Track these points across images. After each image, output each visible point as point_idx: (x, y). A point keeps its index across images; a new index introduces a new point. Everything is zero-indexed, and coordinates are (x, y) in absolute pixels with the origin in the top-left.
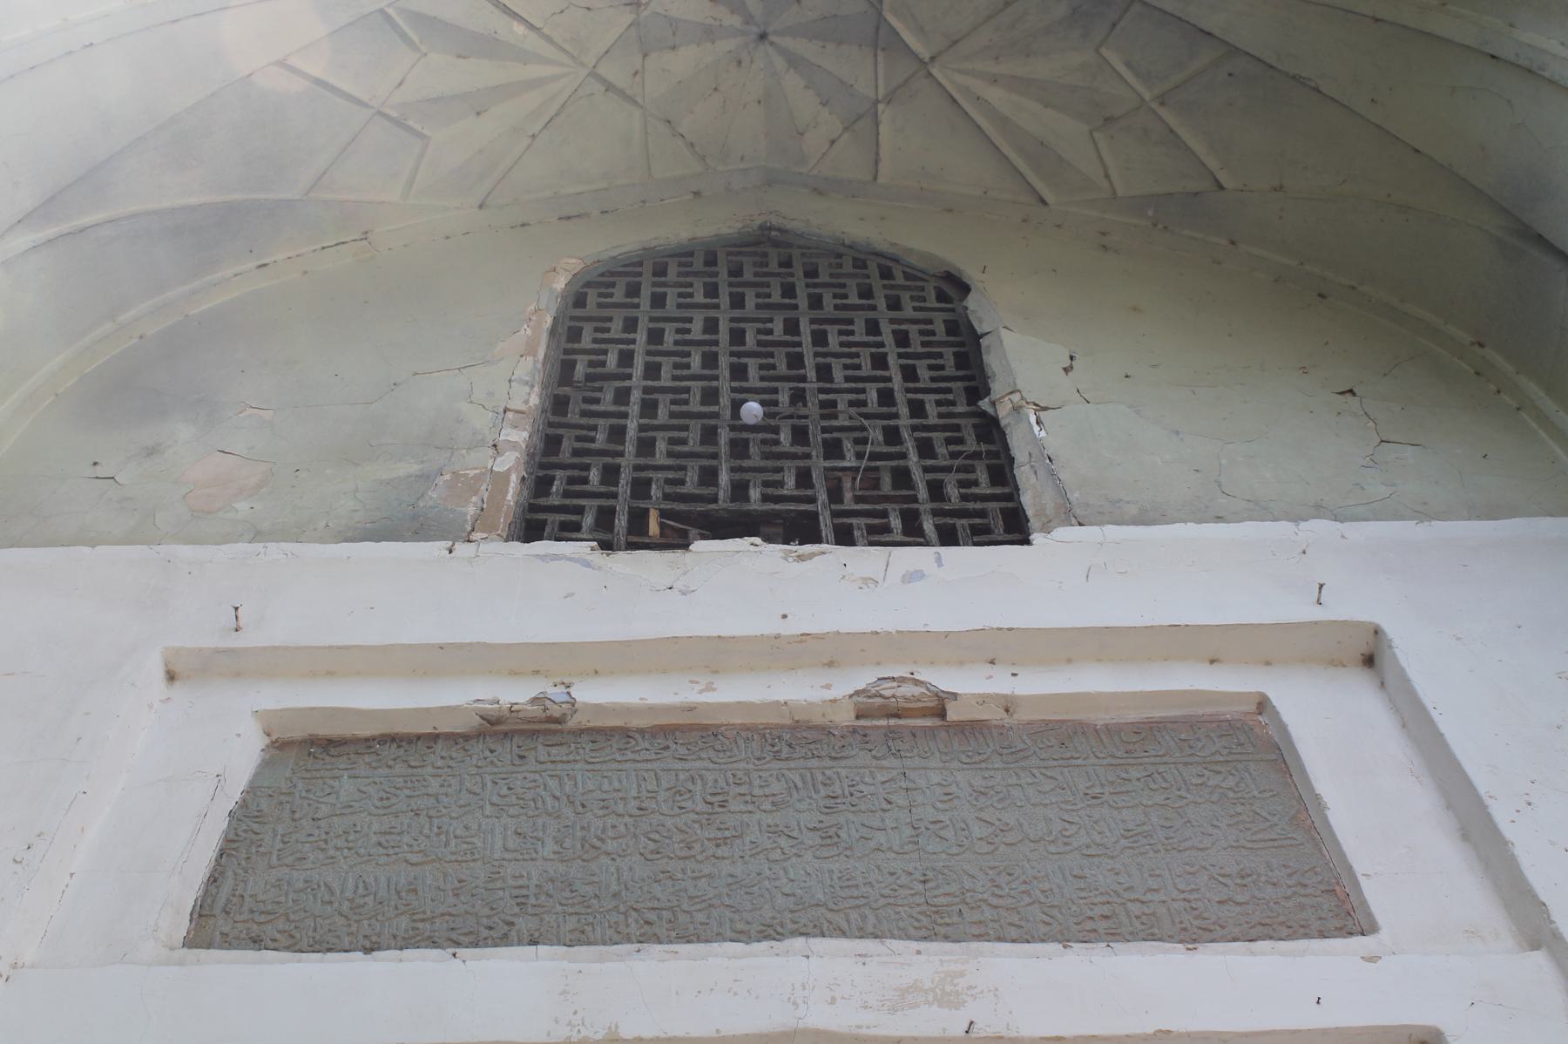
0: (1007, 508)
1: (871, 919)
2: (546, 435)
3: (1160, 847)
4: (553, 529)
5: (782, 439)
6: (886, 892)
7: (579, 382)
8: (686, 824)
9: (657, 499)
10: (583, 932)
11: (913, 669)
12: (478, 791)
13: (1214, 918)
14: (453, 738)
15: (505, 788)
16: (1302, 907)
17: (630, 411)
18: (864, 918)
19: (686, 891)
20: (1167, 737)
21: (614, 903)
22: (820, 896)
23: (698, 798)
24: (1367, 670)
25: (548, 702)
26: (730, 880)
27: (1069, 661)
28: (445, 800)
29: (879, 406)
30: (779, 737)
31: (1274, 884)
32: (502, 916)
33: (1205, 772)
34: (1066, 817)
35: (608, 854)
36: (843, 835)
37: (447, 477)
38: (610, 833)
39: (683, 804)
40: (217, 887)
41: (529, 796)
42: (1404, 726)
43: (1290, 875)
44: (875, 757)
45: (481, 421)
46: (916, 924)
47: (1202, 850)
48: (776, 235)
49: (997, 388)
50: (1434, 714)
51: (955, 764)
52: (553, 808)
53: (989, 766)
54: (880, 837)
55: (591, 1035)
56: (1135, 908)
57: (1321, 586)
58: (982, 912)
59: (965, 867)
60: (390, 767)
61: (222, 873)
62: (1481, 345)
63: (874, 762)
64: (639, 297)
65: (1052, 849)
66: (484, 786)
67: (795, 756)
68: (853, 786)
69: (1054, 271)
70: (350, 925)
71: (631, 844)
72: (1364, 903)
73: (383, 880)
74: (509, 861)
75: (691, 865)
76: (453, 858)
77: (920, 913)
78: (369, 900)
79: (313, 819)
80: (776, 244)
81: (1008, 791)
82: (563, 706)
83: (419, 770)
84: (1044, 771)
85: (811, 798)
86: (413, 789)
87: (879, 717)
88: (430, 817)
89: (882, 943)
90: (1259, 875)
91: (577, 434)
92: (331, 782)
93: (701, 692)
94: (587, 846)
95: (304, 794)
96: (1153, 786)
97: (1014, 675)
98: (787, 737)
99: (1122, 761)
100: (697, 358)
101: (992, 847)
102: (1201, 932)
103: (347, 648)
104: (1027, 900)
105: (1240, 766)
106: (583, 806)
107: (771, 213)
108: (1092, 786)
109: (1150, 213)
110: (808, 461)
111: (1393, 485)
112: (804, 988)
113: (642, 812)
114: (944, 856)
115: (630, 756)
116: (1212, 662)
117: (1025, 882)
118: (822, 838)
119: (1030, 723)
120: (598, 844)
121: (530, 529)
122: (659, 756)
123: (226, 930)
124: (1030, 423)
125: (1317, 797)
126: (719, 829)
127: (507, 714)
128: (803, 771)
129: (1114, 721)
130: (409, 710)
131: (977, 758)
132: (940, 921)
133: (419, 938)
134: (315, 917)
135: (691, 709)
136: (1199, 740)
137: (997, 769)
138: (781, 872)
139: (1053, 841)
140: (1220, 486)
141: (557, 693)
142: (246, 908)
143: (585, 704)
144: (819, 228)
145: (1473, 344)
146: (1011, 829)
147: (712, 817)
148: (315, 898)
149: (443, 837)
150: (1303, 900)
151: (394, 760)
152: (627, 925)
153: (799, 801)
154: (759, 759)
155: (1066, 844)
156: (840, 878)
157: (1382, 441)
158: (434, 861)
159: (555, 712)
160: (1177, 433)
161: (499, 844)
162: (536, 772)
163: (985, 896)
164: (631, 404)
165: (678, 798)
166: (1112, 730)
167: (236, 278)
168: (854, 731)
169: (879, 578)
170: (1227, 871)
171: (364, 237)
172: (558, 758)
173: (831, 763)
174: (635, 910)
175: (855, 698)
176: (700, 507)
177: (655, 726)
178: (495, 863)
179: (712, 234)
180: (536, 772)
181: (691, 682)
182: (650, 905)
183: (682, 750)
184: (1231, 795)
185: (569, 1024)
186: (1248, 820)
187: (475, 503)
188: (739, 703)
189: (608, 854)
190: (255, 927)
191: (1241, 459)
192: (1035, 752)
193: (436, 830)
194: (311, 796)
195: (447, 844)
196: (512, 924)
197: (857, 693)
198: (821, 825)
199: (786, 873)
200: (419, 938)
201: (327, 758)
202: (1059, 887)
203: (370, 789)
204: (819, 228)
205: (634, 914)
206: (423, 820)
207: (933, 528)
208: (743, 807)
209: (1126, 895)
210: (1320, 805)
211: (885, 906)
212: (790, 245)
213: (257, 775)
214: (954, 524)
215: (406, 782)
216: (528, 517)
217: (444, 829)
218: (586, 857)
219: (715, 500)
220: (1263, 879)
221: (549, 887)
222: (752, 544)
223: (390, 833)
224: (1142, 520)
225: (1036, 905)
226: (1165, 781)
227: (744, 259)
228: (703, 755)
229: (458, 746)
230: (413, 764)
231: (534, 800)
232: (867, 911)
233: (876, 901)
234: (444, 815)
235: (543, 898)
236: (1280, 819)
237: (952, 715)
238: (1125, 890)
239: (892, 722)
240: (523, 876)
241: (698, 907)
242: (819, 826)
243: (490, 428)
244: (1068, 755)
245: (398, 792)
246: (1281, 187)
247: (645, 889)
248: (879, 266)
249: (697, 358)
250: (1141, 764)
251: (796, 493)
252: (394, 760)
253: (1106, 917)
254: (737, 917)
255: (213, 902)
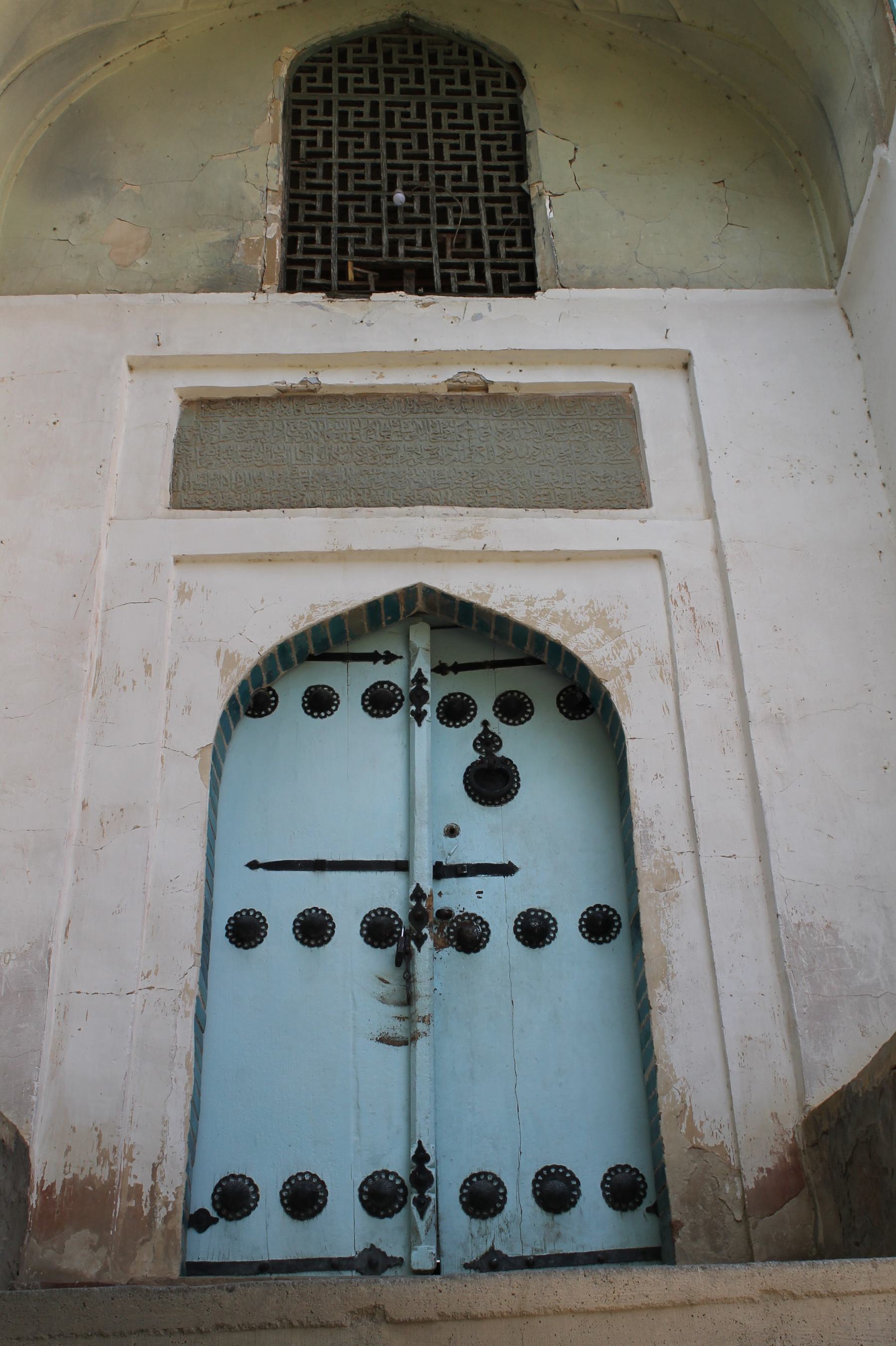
0: (529, 263)
1: (450, 494)
2: (290, 204)
3: (573, 462)
4: (301, 276)
5: (415, 207)
6: (457, 481)
7: (303, 159)
8: (373, 447)
9: (352, 254)
10: (333, 499)
11: (475, 367)
12: (281, 429)
13: (589, 497)
14: (267, 400)
15: (293, 428)
16: (626, 492)
17: (333, 184)
18: (447, 493)
19: (374, 480)
20: (586, 405)
21: (344, 486)
22: (429, 483)
23: (378, 433)
24: (683, 370)
25: (308, 383)
26: (393, 475)
27: (547, 364)
28: (267, 433)
29: (469, 181)
30: (413, 401)
31: (617, 482)
32: (299, 491)
33: (600, 424)
34: (536, 446)
35: (341, 462)
36: (440, 454)
37: (243, 242)
38: (341, 451)
39: (371, 437)
40: (177, 478)
41: (304, 432)
42: (691, 404)
43: (625, 478)
44: (455, 413)
45: (255, 197)
46: (469, 497)
47: (591, 464)
48: (412, 23)
49: (532, 174)
50: (701, 404)
51: (491, 417)
52: (315, 438)
53: (505, 418)
54: (456, 454)
55: (342, 549)
56: (558, 491)
57: (667, 331)
58: (495, 492)
59: (490, 470)
60: (240, 416)
61: (178, 471)
62: (800, 155)
63: (455, 415)
64: (331, 82)
65: (528, 462)
66: (283, 426)
67: (420, 411)
68: (445, 428)
69: (577, 66)
70: (237, 496)
71: (350, 457)
72: (650, 493)
73: (246, 474)
74: (299, 465)
75: (375, 467)
76: (275, 463)
77: (470, 492)
78: (243, 484)
79: (211, 444)
80: (414, 32)
81: (512, 432)
82: (316, 385)
83: (253, 417)
84: (529, 421)
85: (426, 434)
86: (252, 428)
87: (459, 391)
88: (262, 443)
89: (454, 508)
90: (612, 477)
91: (306, 203)
92: (215, 424)
93: (377, 378)
94: (331, 458)
95: (204, 430)
96: (576, 431)
97: (521, 371)
98: (416, 401)
99: (564, 417)
100: (367, 138)
101: (502, 460)
102: (583, 503)
103: (213, 355)
104: (514, 486)
105: (616, 421)
106: (328, 437)
107: (409, 4)
108: (549, 430)
109: (639, 25)
110: (428, 225)
111: (725, 258)
112: (422, 531)
113: (354, 441)
114: (482, 464)
115: (347, 410)
116: (613, 365)
117: (514, 478)
118: (430, 454)
119: (526, 395)
120: (335, 456)
121: (289, 285)
122: (360, 411)
123: (186, 498)
124: (545, 207)
125: (643, 441)
126: (387, 450)
127: (290, 388)
128: (423, 420)
129: (564, 395)
130: (245, 387)
131: (501, 414)
132: (478, 495)
133: (266, 502)
134: (222, 492)
135: (373, 387)
136: (600, 406)
137: (508, 420)
138: (413, 471)
139: (528, 458)
140: (636, 256)
141: (311, 377)
142: (192, 488)
143: (325, 384)
144: (439, 19)
145: (796, 152)
146: (511, 452)
147: (384, 443)
148: (220, 483)
149: (269, 453)
150: (627, 489)
151: (241, 412)
152: (351, 496)
153: (422, 435)
154: (404, 413)
155: (534, 459)
156: (438, 475)
157: (728, 224)
158: (267, 465)
159: (312, 387)
160: (623, 213)
161: (294, 457)
162: (305, 419)
163: (497, 484)
164: (333, 178)
165: (369, 433)
166: (562, 400)
167: (94, 75)
168: (446, 398)
169: (461, 317)
170: (599, 475)
171: (163, 35)
172: (315, 412)
173: (436, 415)
174: (353, 489)
175: (448, 382)
176: (374, 260)
177: (357, 394)
178: (293, 466)
179: (373, 22)
180: (305, 419)
181: (373, 372)
182: (359, 486)
183: (370, 408)
184: (609, 436)
185: (333, 544)
186: (613, 449)
187: (261, 261)
188: (395, 384)
189: (341, 462)
190: (198, 497)
191: (651, 235)
192: (526, 411)
193: (265, 449)
194: (208, 431)
195: (271, 457)
196: (303, 495)
197: (449, 380)
198: (431, 448)
199: (416, 472)
200: (266, 502)
201: (211, 411)
202: (528, 480)
203: (234, 428)
204: (439, 19)
205: (353, 490)
206: (259, 444)
207: (490, 275)
208: (397, 438)
209: (555, 485)
210: (644, 446)
211: (456, 488)
212: (420, 33)
213: (180, 420)
214: (501, 274)
215: (248, 424)
216: (288, 268)
217: (269, 449)
218: (331, 463)
219: (379, 254)
220: (613, 479)
221: (317, 477)
222: (400, 296)
223: (246, 451)
224: (592, 284)
225: (518, 489)
226: (581, 428)
227: (393, 46)
228: (379, 410)
229: (270, 405)
230: (250, 414)
231: (306, 434)
232: (448, 490)
233: (452, 486)
234: (268, 442)
235: (315, 483)
236: (627, 450)
237: (491, 390)
238: (555, 483)
239: (464, 393)
240: (305, 473)
241: (379, 487)
242: (429, 448)
243: (261, 204)
244: (541, 413)
245: (246, 429)
246: (712, 28)
247: (357, 479)
248: (475, 52)
249: (367, 138)
250: (572, 419)
251: (422, 250)
252: (241, 412)
253: (545, 495)
254: (395, 492)
255: (177, 484)
